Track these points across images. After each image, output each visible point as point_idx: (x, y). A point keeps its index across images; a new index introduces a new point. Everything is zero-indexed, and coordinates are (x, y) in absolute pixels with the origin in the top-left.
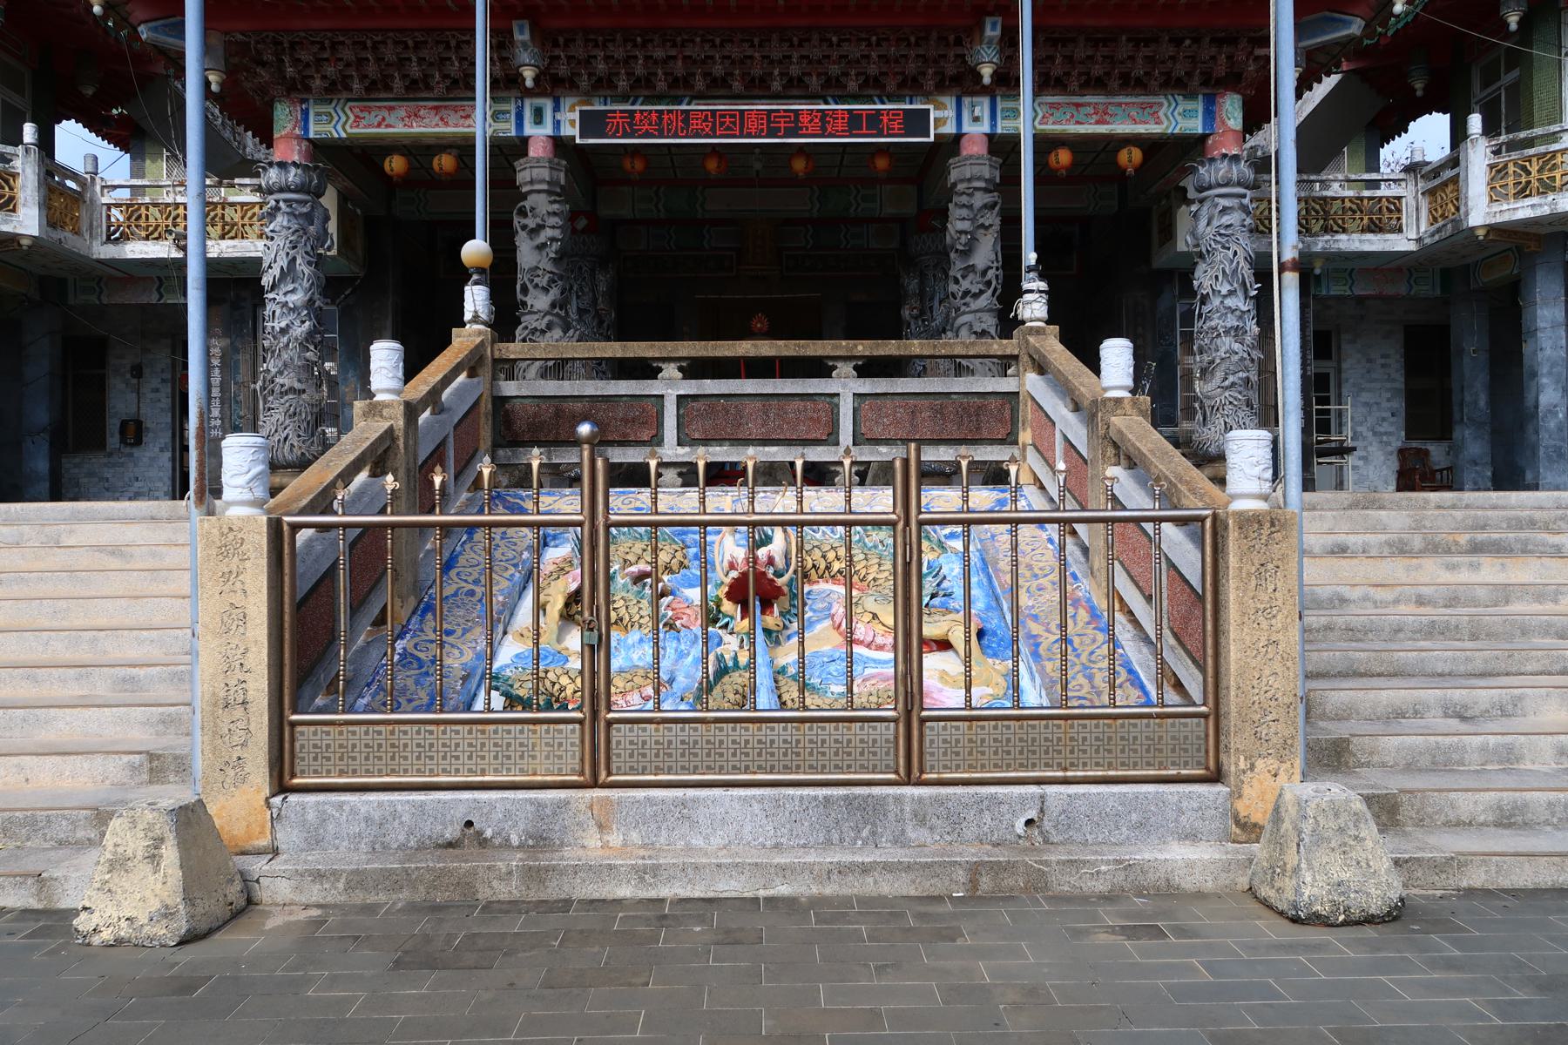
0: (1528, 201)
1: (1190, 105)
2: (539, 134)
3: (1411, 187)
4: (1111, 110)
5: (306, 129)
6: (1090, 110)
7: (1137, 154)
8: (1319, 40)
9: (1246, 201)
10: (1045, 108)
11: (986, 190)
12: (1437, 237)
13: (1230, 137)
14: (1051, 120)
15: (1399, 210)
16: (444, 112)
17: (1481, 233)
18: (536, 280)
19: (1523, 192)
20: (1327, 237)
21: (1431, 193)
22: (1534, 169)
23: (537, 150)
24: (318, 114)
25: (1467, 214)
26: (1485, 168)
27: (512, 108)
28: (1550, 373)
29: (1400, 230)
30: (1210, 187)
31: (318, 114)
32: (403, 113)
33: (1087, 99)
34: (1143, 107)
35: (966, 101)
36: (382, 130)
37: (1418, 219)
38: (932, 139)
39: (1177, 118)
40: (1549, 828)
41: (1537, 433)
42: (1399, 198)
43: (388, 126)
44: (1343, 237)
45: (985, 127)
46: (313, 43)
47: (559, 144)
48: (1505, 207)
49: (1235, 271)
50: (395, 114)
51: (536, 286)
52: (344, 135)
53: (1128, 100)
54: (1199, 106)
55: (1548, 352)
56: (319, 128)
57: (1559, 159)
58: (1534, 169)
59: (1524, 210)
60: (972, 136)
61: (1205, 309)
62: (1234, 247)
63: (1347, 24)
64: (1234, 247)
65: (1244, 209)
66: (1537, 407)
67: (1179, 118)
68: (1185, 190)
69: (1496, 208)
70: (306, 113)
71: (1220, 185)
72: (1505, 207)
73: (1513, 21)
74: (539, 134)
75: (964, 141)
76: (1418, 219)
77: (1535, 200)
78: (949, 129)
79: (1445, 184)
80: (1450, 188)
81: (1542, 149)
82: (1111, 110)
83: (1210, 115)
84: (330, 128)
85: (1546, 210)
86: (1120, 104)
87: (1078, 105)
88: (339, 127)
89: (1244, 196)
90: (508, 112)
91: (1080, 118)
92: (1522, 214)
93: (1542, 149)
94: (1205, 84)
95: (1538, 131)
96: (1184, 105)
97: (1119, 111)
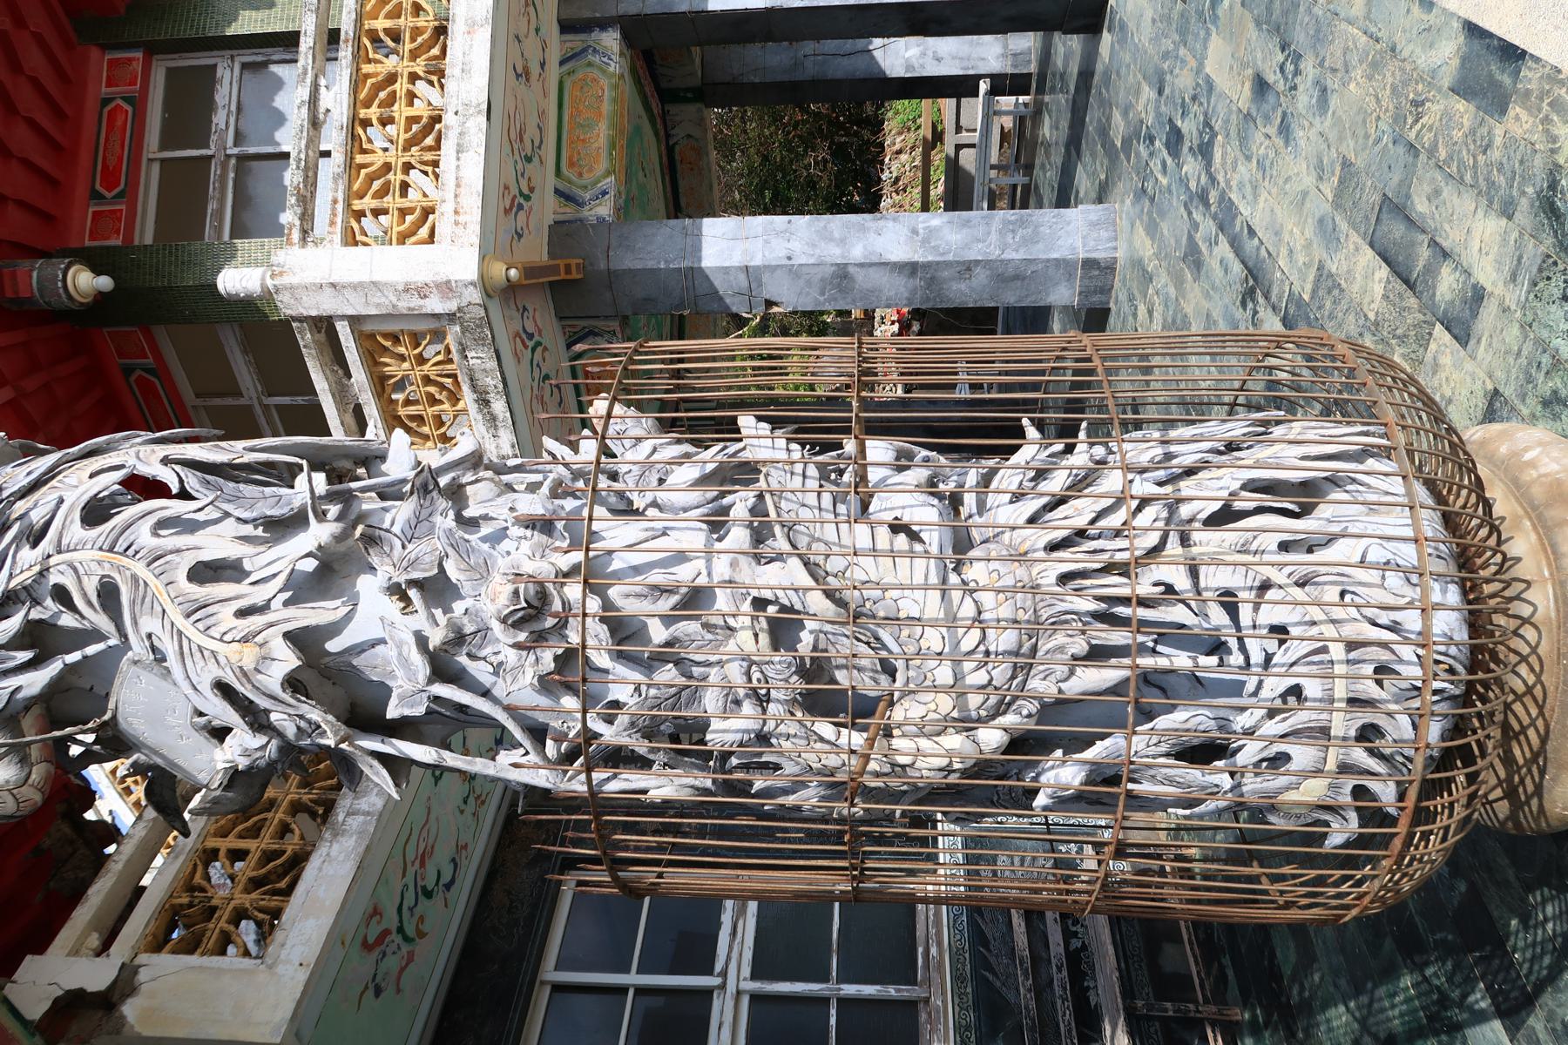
12: (499, 406)
28: (842, 241)
41: (968, 267)
55: (796, 246)
66: (911, 268)
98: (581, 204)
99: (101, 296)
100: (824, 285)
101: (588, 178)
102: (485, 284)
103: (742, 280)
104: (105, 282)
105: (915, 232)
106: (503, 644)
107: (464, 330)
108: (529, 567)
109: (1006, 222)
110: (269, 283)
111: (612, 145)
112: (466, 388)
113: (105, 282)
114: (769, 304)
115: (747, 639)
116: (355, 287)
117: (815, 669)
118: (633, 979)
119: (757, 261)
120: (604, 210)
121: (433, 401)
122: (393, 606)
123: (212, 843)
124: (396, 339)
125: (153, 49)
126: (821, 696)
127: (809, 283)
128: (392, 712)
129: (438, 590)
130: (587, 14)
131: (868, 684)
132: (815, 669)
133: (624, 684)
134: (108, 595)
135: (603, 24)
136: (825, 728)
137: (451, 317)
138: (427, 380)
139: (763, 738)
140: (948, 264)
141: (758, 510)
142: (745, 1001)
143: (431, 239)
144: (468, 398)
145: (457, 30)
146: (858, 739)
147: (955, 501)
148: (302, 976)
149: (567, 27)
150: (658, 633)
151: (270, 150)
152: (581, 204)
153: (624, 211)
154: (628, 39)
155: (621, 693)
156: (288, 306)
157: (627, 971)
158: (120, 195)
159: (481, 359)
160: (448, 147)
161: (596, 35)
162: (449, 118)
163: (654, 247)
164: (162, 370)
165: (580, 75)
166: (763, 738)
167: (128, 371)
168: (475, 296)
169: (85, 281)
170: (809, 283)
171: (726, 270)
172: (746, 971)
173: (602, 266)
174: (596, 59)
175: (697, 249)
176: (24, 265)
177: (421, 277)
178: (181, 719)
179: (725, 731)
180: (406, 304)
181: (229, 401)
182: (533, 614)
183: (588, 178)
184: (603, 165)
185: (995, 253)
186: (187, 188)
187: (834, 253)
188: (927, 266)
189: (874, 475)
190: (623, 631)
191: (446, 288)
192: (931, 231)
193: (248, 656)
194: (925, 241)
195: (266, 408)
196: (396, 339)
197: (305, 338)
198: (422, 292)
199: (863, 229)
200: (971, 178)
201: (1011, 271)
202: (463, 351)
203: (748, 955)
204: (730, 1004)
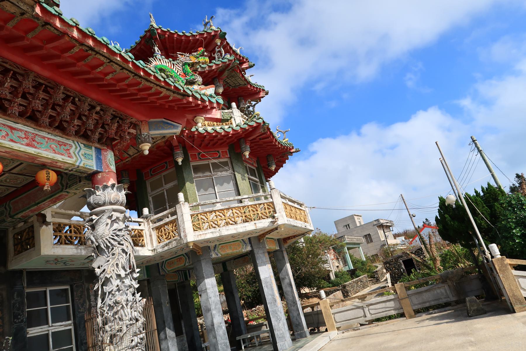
1: (88, 151)
4: (38, 139)
7: (53, 177)
8: (161, 132)
12: (166, 248)
15: (142, 236)
21: (158, 228)
28: (216, 308)
30: (104, 204)
33: (19, 126)
34: (60, 144)
39: (79, 156)
41: (215, 337)
42: (142, 230)
48: (201, 233)
53: (49, 136)
55: (213, 299)
61: (107, 289)
63: (175, 127)
66: (213, 325)
67: (82, 157)
68: (44, 216)
69: (197, 233)
71: (111, 204)
72: (201, 233)
82: (38, 139)
83: (99, 160)
85: (217, 235)
86: (44, 138)
87: (12, 128)
91: (14, 138)
94: (100, 141)
97: (44, 141)
98: (214, 251)
99: (177, 163)
100: (206, 307)
101: (220, 251)
102: (187, 244)
103: (204, 289)
104: (180, 164)
105: (221, 323)
106: (113, 300)
107: (179, 240)
108: (122, 301)
109: (226, 343)
110: (181, 203)
111: (227, 254)
112: (169, 241)
113: (180, 164)
114: (201, 295)
115: (117, 327)
116: (183, 219)
117: (115, 335)
118: (49, 307)
119: (208, 291)
120: (214, 256)
121: (165, 234)
122: (116, 285)
123: (72, 226)
124: (175, 226)
125: (230, 158)
126: (112, 337)
127: (206, 303)
128: (104, 287)
129: (119, 290)
130: (252, 243)
131: (114, 342)
132: (115, 335)
133: (111, 314)
134: (113, 254)
135: (251, 246)
136: (109, 338)
137: (181, 237)
138: (169, 233)
139: (107, 332)
140: (215, 332)
141: (133, 324)
142: (47, 332)
143: (194, 230)
144: (167, 241)
145: (235, 226)
146: (108, 342)
147: (137, 346)
148: (52, 254)
149: (249, 239)
150: (117, 316)
151: (215, 184)
152: (214, 251)
153: (213, 260)
154: (251, 251)
155: (109, 314)
156: (178, 206)
157: (51, 305)
158: (200, 159)
159: (174, 244)
160: (213, 230)
161: (249, 245)
162: (218, 229)
163: (207, 268)
164: (167, 169)
165: (241, 244)
166: (107, 332)
167: (166, 163)
168: (185, 242)
169: (180, 160)
170: (206, 303)
171: (205, 285)
172: (53, 331)
173: (202, 259)
174: (244, 246)
175: (208, 277)
176: (181, 149)
177: (187, 231)
178: (101, 264)
179: (107, 327)
180: (181, 228)
181: (163, 182)
182: (117, 303)
183: (220, 251)
184: (223, 253)
185: (219, 343)
186: (205, 168)
187: (213, 307)
188: (214, 328)
189: (139, 336)
190: (116, 313)
191: (186, 236)
192: (221, 327)
193: (108, 272)
194: (219, 326)
195: (163, 190)
196: (175, 226)
197: (172, 210)
198: (184, 231)
199: (219, 312)
200: (260, 330)
201: (216, 347)
202: (175, 240)
203: (56, 330)
204: (46, 329)
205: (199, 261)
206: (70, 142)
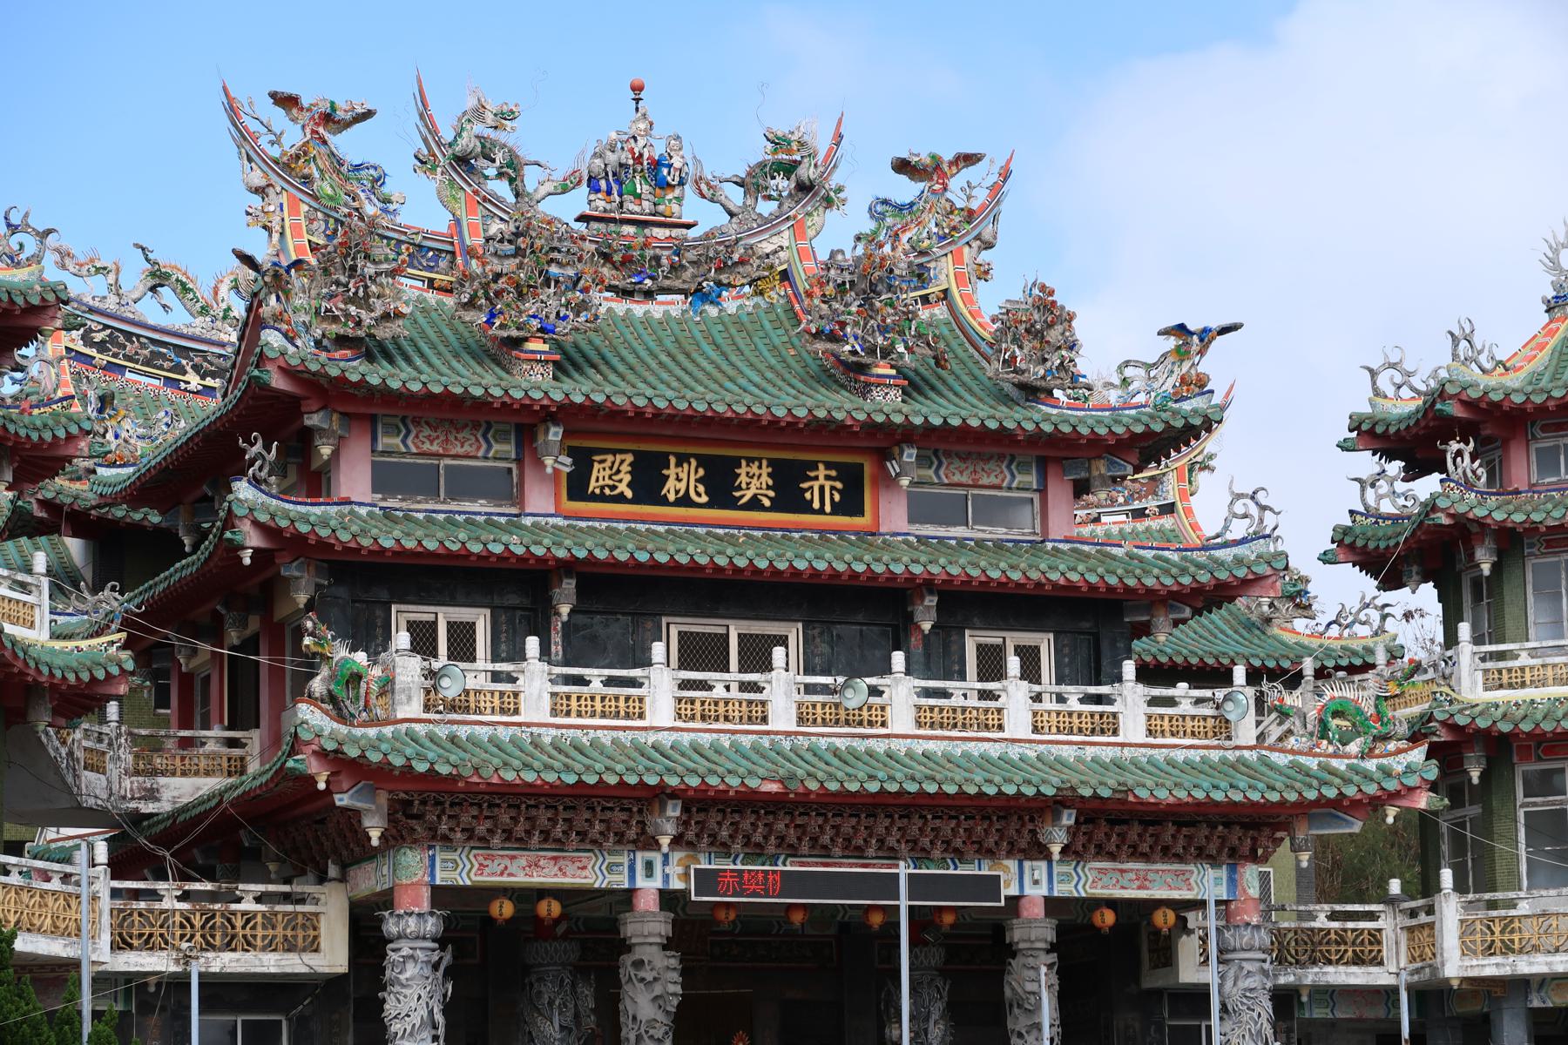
0: (1494, 960)
2: (649, 886)
3: (1390, 920)
4: (1151, 876)
5: (433, 875)
6: (1132, 876)
9: (1266, 966)
10: (1095, 873)
11: (1048, 952)
13: (1251, 905)
14: (1100, 884)
15: (1379, 943)
16: (562, 863)
17: (1455, 984)
18: (652, 1032)
19: (1489, 950)
20: (1316, 970)
21: (1410, 930)
22: (1497, 929)
23: (647, 902)
24: (444, 861)
25: (1443, 964)
26: (1456, 923)
27: (625, 859)
29: (1381, 963)
30: (1234, 950)
31: (444, 861)
32: (523, 862)
33: (1130, 865)
34: (1177, 874)
35: (1027, 864)
36: (505, 879)
37: (1397, 953)
38: (1003, 903)
40: (1341, 674)
42: (1379, 930)
43: (510, 875)
44: (1330, 969)
45: (1043, 890)
46: (472, 804)
47: (669, 899)
48: (1475, 962)
49: (1259, 1032)
50: (516, 863)
51: (651, 1037)
52: (468, 883)
53: (1165, 867)
54: (1223, 873)
56: (446, 875)
57: (1516, 924)
58: (1497, 929)
59: (1491, 967)
60: (1032, 899)
62: (1258, 1009)
64: (1258, 1009)
65: (1265, 973)
70: (432, 859)
72: (1475, 962)
73: (1475, 775)
74: (649, 886)
75: (1023, 901)
76: (1397, 953)
77: (1498, 959)
78: (1013, 890)
79: (1422, 926)
80: (1426, 932)
81: (1503, 913)
82: (1151, 876)
83: (1232, 882)
84: (455, 875)
85: (1506, 971)
86: (1157, 871)
87: (1122, 871)
88: (464, 875)
89: (1264, 961)
90: (621, 864)
91: (1125, 883)
92: (1489, 972)
93: (1503, 913)
95: (1499, 895)
96: (1211, 873)
97: (1157, 877)
120: (1536, 1003)
205: (1500, 1010)
206: (1191, 867)
